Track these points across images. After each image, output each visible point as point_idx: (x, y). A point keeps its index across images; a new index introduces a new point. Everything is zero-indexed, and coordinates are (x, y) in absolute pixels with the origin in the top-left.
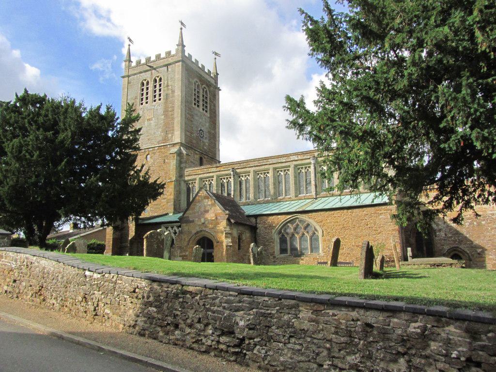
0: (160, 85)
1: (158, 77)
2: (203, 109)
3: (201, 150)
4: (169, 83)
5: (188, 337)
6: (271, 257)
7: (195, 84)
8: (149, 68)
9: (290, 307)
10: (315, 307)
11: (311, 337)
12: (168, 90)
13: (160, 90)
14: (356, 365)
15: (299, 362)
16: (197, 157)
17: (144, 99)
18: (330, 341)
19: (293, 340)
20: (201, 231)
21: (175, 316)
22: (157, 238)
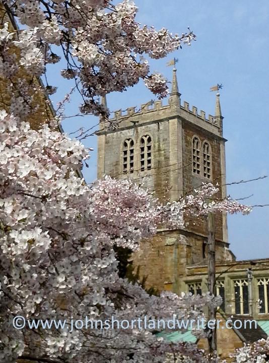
0: (149, 148)
1: (146, 136)
2: (205, 175)
4: (161, 146)
12: (160, 157)
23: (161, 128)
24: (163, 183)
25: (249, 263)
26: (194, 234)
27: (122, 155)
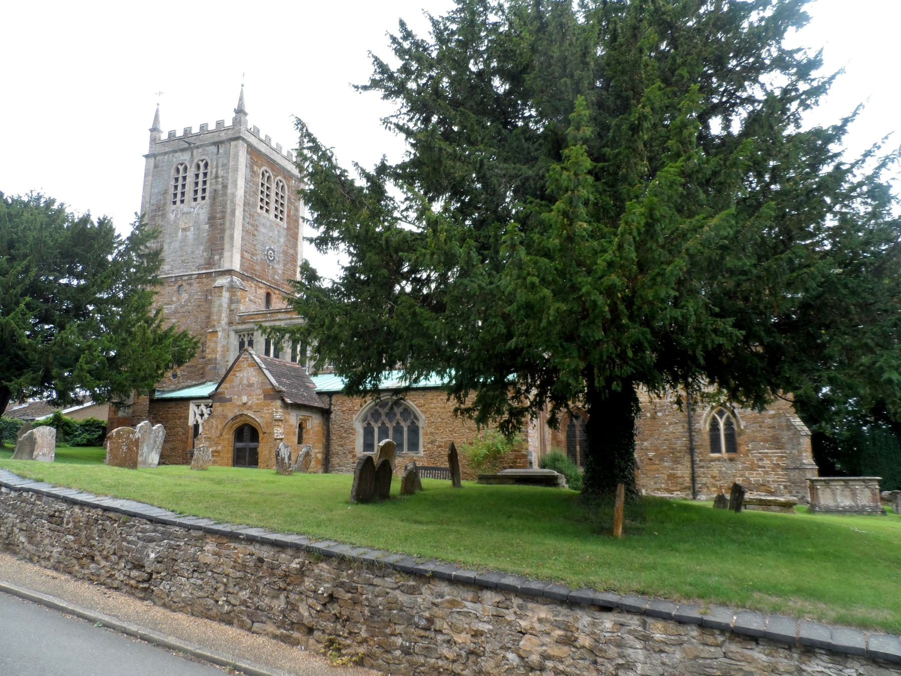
0: (205, 174)
2: (276, 216)
3: (268, 281)
5: (103, 571)
6: (350, 456)
7: (263, 174)
8: (186, 145)
9: (197, 539)
10: (219, 541)
11: (212, 571)
13: (205, 183)
14: (245, 601)
15: (198, 598)
16: (262, 292)
17: (179, 196)
18: (227, 575)
19: (196, 574)
20: (241, 415)
21: (92, 546)
22: (128, 438)
23: (221, 151)
24: (218, 215)
25: (817, 650)
26: (252, 278)
27: (173, 182)
